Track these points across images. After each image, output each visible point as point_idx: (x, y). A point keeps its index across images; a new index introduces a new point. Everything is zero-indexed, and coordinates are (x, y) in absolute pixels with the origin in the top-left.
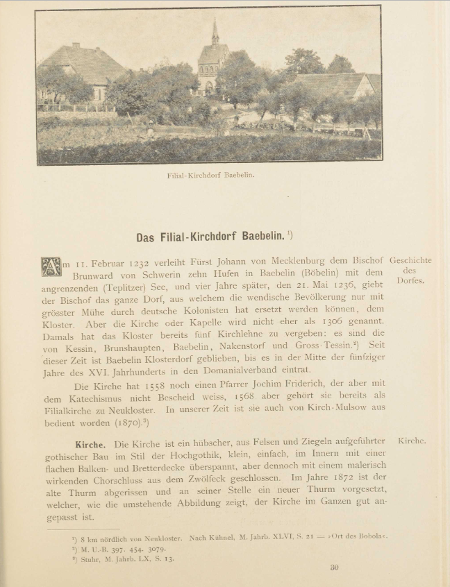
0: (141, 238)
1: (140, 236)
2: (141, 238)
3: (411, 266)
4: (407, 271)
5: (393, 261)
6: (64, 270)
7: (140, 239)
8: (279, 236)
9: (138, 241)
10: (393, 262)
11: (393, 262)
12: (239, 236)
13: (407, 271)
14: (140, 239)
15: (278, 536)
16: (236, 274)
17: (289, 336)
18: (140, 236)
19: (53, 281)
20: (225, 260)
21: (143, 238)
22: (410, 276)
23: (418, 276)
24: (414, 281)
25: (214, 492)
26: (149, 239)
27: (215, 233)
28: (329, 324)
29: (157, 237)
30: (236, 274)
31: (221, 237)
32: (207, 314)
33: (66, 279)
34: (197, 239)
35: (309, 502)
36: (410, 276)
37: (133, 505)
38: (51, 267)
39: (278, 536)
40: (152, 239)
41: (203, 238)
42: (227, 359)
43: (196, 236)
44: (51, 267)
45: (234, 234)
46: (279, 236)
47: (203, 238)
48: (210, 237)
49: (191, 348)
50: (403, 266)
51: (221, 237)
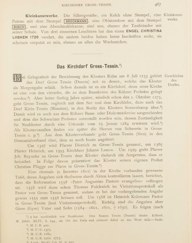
0: (59, 67)
1: (58, 66)
2: (59, 67)
3: (174, 78)
4: (173, 80)
5: (166, 76)
6: (23, 79)
7: (58, 67)
8: (116, 66)
9: (58, 68)
10: (166, 76)
11: (166, 76)
12: (89, 66)
13: (173, 80)
14: (58, 67)
15: (35, 221)
16: (92, 37)
17: (120, 192)
18: (58, 66)
19: (18, 84)
20: (68, 207)
21: (60, 67)
22: (174, 83)
23: (177, 83)
24: (176, 85)
25: (117, 26)
26: (62, 67)
27: (78, 65)
28: (157, 146)
29: (66, 67)
30: (92, 37)
31: (81, 67)
32: (127, 17)
33: (24, 82)
34: (70, 67)
35: (97, 42)
36: (174, 83)
37: (22, 141)
38: (18, 78)
39: (35, 221)
40: (64, 67)
41: (73, 67)
42: (112, 26)
43: (70, 66)
44: (18, 78)
45: (86, 66)
46: (116, 66)
47: (73, 67)
48: (76, 67)
49: (111, 26)
50: (171, 78)
51: (81, 67)
